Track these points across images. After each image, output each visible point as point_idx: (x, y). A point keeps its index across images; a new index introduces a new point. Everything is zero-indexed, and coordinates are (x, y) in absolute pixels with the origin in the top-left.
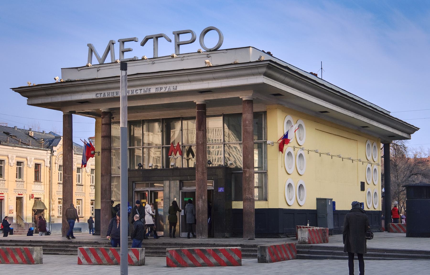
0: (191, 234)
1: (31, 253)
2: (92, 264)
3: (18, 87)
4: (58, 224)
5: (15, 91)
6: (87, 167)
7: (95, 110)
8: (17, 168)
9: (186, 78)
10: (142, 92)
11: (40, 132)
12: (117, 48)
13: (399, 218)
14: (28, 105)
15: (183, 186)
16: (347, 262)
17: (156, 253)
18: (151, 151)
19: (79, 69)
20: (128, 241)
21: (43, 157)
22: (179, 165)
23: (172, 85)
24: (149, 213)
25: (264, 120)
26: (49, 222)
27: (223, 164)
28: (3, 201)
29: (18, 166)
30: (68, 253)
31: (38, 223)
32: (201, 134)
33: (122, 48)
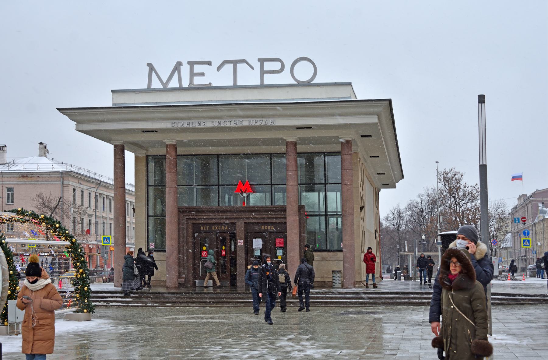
1: (298, 272)
4: (110, 130)
5: (63, 113)
6: (344, 242)
7: (100, 289)
8: (8, 194)
10: (232, 124)
12: (185, 70)
13: (481, 272)
14: (77, 130)
16: (329, 210)
17: (518, 304)
23: (270, 119)
26: (35, 299)
29: (10, 192)
32: (281, 109)
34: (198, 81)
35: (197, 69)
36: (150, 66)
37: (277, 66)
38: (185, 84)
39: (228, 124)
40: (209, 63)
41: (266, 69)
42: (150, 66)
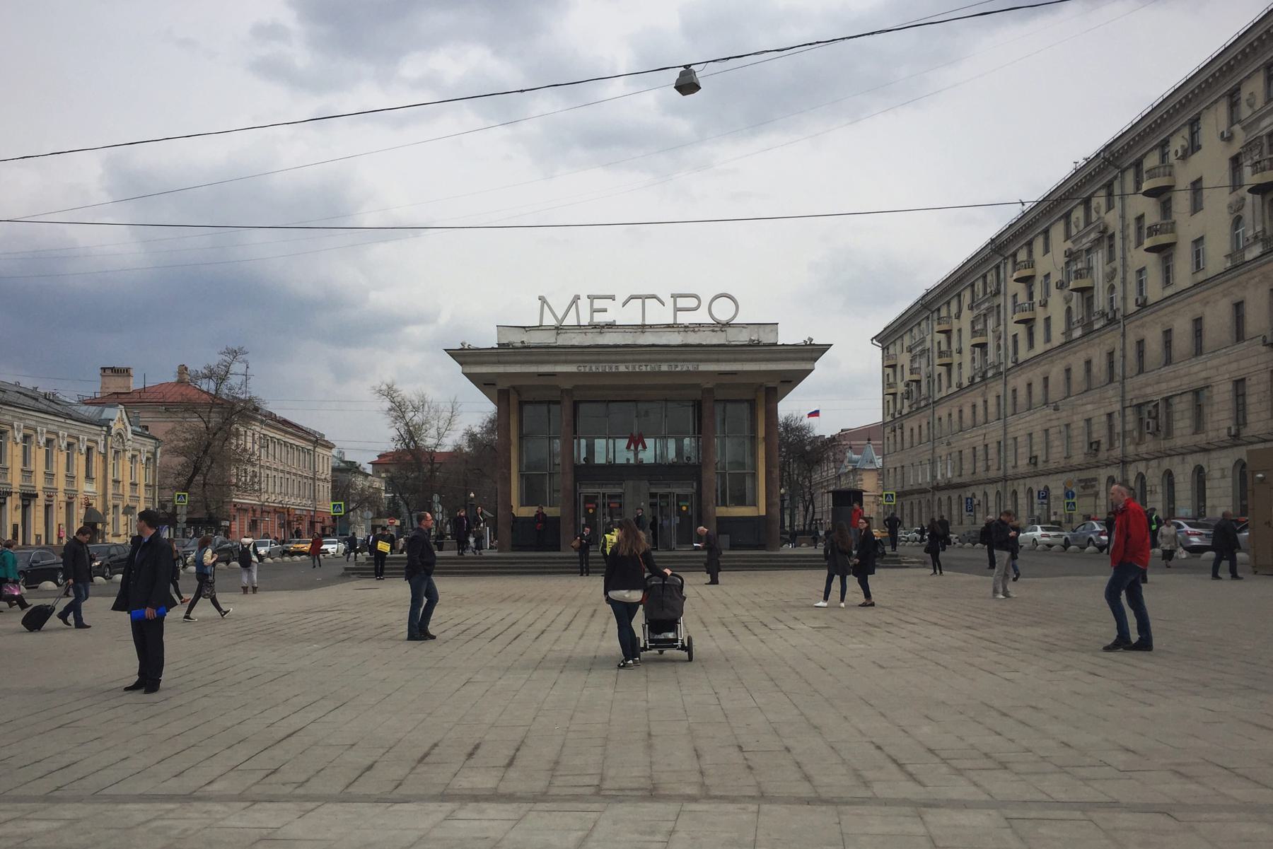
3: (882, 330)
10: (649, 369)
12: (584, 304)
15: (30, 545)
18: (1097, 252)
19: (527, 329)
21: (547, 807)
25: (550, 480)
27: (1060, 484)
30: (938, 291)
31: (11, 440)
33: (831, 454)
34: (600, 318)
35: (598, 304)
37: (692, 303)
38: (585, 321)
39: (644, 369)
40: (612, 298)
41: (679, 306)
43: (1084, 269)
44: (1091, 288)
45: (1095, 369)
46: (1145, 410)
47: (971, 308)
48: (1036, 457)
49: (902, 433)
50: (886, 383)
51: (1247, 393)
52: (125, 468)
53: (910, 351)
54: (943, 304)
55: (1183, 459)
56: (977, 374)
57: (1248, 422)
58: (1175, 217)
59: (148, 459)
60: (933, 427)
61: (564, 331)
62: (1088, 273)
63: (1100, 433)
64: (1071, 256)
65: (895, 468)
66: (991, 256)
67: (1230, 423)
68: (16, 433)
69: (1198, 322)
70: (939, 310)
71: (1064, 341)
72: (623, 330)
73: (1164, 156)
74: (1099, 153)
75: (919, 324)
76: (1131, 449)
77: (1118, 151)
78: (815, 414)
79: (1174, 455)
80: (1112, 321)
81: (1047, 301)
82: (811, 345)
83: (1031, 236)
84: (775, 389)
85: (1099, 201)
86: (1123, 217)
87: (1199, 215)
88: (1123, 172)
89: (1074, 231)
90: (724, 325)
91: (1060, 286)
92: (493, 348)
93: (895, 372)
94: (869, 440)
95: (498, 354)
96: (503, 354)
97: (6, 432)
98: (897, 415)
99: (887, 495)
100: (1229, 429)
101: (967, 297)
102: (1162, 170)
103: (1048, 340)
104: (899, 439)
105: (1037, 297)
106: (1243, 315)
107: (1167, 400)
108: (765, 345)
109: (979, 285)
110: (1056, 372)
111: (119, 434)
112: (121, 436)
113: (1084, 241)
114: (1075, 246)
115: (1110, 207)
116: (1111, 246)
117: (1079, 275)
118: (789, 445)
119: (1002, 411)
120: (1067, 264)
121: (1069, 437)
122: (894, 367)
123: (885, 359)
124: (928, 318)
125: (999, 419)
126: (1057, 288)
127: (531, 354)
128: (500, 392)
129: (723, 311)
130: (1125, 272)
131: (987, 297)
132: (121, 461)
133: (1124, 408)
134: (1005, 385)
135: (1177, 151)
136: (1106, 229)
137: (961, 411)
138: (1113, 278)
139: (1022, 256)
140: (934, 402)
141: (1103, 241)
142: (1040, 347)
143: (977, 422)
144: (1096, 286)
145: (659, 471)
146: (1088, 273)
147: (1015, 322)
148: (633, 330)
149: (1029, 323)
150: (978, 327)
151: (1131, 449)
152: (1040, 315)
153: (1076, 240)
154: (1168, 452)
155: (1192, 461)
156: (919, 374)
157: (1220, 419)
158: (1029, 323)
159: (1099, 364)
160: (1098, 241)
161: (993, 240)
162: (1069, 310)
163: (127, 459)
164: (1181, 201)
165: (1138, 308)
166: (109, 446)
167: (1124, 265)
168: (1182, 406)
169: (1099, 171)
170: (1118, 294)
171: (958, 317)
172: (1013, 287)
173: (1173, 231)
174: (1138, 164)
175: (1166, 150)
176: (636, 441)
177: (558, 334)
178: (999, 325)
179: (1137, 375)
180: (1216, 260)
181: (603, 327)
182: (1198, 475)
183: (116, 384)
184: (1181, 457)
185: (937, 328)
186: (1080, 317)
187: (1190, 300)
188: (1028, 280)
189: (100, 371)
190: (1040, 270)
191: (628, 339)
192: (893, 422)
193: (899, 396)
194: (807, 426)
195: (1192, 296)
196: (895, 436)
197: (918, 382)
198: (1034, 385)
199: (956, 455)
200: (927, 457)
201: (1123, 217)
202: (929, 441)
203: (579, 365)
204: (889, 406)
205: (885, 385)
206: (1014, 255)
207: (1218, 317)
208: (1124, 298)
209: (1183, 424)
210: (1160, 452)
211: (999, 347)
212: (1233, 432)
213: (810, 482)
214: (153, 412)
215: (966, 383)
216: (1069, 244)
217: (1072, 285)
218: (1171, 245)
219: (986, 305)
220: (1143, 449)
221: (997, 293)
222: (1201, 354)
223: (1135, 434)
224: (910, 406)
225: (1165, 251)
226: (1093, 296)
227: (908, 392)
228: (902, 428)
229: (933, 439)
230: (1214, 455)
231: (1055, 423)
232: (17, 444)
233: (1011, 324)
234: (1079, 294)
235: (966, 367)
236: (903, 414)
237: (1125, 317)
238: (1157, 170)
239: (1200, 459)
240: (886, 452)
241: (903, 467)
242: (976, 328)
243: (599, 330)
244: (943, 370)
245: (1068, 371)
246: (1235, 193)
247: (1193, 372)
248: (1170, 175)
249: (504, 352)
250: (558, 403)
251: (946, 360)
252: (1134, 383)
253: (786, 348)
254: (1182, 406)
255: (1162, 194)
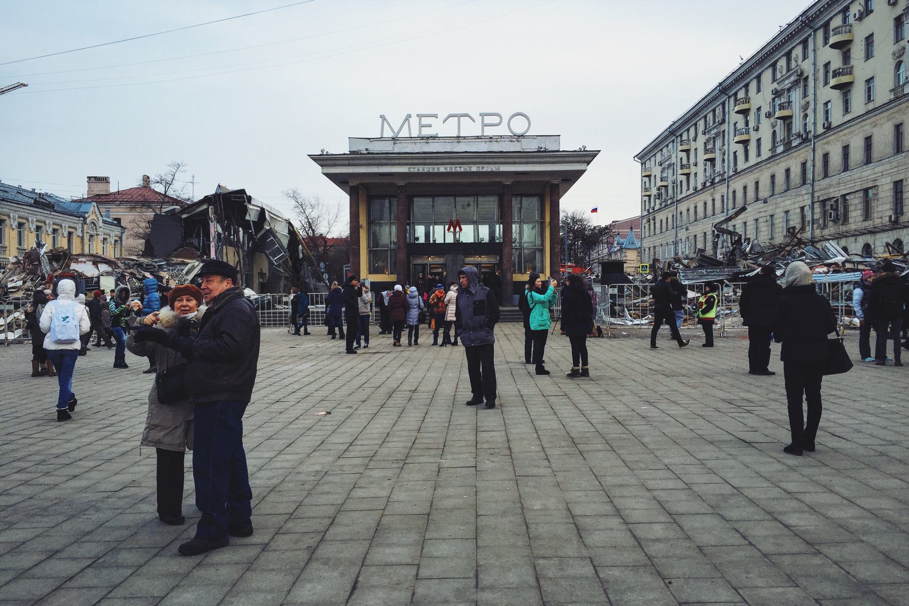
0: (665, 329)
2: (592, 335)
9: (511, 160)
10: (462, 170)
11: (306, 561)
12: (414, 121)
20: (820, 284)
21: (126, 446)
22: (440, 240)
24: (358, 577)
28: (285, 330)
30: (681, 121)
31: (44, 232)
34: (426, 132)
35: (425, 121)
36: (383, 118)
37: (496, 120)
40: (436, 116)
42: (383, 118)
43: (785, 103)
44: (791, 117)
45: (792, 176)
46: (828, 204)
47: (704, 133)
48: (749, 239)
49: (655, 223)
50: (643, 187)
51: (904, 190)
52: (98, 247)
53: (661, 165)
54: (685, 131)
55: (856, 239)
56: (708, 180)
57: (904, 211)
58: (853, 62)
59: (116, 241)
60: (677, 218)
61: (398, 142)
62: (789, 105)
63: (795, 222)
64: (777, 94)
65: (649, 248)
66: (719, 95)
67: (890, 213)
68: (12, 221)
69: (868, 140)
70: (681, 135)
71: (770, 155)
72: (443, 141)
73: (845, 19)
74: (799, 17)
75: (667, 146)
76: (818, 232)
77: (812, 15)
78: (595, 210)
79: (849, 236)
80: (806, 140)
81: (758, 127)
82: (584, 151)
83: (748, 80)
84: (557, 186)
85: (798, 51)
86: (815, 64)
87: (871, 61)
88: (815, 31)
89: (778, 76)
90: (519, 136)
91: (769, 115)
92: (344, 154)
93: (650, 180)
94: (631, 228)
95: (348, 159)
96: (352, 159)
97: (4, 221)
98: (651, 211)
99: (642, 266)
100: (890, 217)
101: (701, 126)
102: (844, 29)
103: (759, 155)
104: (652, 227)
105: (752, 124)
106: (902, 133)
107: (844, 196)
108: (550, 152)
109: (710, 116)
110: (765, 179)
111: (93, 223)
112: (95, 225)
113: (787, 82)
114: (780, 86)
115: (805, 57)
116: (806, 86)
117: (782, 107)
118: (573, 231)
119: (725, 207)
120: (773, 99)
121: (772, 224)
122: (649, 176)
123: (643, 170)
124: (673, 141)
125: (723, 212)
126: (766, 117)
127: (374, 159)
128: (351, 188)
129: (519, 126)
130: (815, 104)
131: (715, 125)
132: (94, 242)
133: (813, 203)
134: (728, 187)
135: (855, 14)
136: (802, 73)
137: (696, 207)
138: (806, 109)
139: (741, 94)
140: (677, 201)
141: (800, 82)
142: (753, 160)
143: (707, 215)
144: (794, 116)
145: (476, 248)
146: (789, 105)
147: (736, 143)
148: (450, 141)
149: (745, 143)
150: (710, 146)
151: (818, 232)
152: (754, 136)
153: (781, 82)
154: (845, 234)
155: (862, 241)
156: (667, 181)
157: (883, 210)
158: (745, 143)
159: (796, 171)
160: (796, 83)
161: (720, 84)
162: (774, 133)
163: (99, 240)
164: (858, 50)
165: (825, 130)
166: (85, 231)
167: (815, 100)
168: (856, 203)
169: (798, 31)
170: (810, 120)
171: (695, 140)
172: (735, 118)
173: (851, 73)
174: (826, 25)
175: (847, 14)
176: (455, 224)
177: (395, 144)
178: (724, 145)
179: (823, 179)
180: (882, 94)
181: (428, 138)
182: (867, 250)
183: (99, 189)
184: (854, 238)
185: (680, 148)
186: (782, 138)
187: (864, 123)
188: (745, 112)
189: (87, 179)
190: (754, 105)
191: (448, 148)
192: (649, 215)
193: (652, 197)
194: (587, 218)
195: (864, 120)
196: (649, 225)
197: (666, 187)
198: (748, 187)
199: (691, 238)
200: (671, 240)
201: (815, 64)
202: (673, 228)
203: (410, 167)
204: (645, 204)
205: (643, 190)
206: (736, 94)
207: (883, 136)
208: (815, 124)
209: (856, 214)
210: (839, 234)
211: (723, 160)
212: (893, 219)
213: (589, 258)
214: (124, 208)
215: (700, 187)
216: (775, 85)
217: (778, 114)
218: (850, 84)
219: (715, 131)
220: (826, 232)
221: (723, 121)
222: (871, 163)
223: (821, 222)
224: (661, 204)
225: (845, 88)
226: (792, 122)
227: (659, 195)
228: (654, 219)
229: (676, 227)
230: (878, 236)
231: (763, 214)
232: (13, 229)
233: (732, 143)
234: (782, 121)
235: (700, 176)
236: (655, 209)
237: (815, 137)
238: (840, 29)
239: (869, 239)
240: (643, 237)
241: (655, 247)
242: (708, 148)
243: (425, 141)
244: (684, 178)
245: (773, 177)
246: (897, 44)
247: (860, 176)
248: (850, 32)
249: (354, 157)
250: (394, 196)
251: (686, 171)
252: (821, 184)
253: (565, 153)
254: (856, 203)
255: (844, 47)
